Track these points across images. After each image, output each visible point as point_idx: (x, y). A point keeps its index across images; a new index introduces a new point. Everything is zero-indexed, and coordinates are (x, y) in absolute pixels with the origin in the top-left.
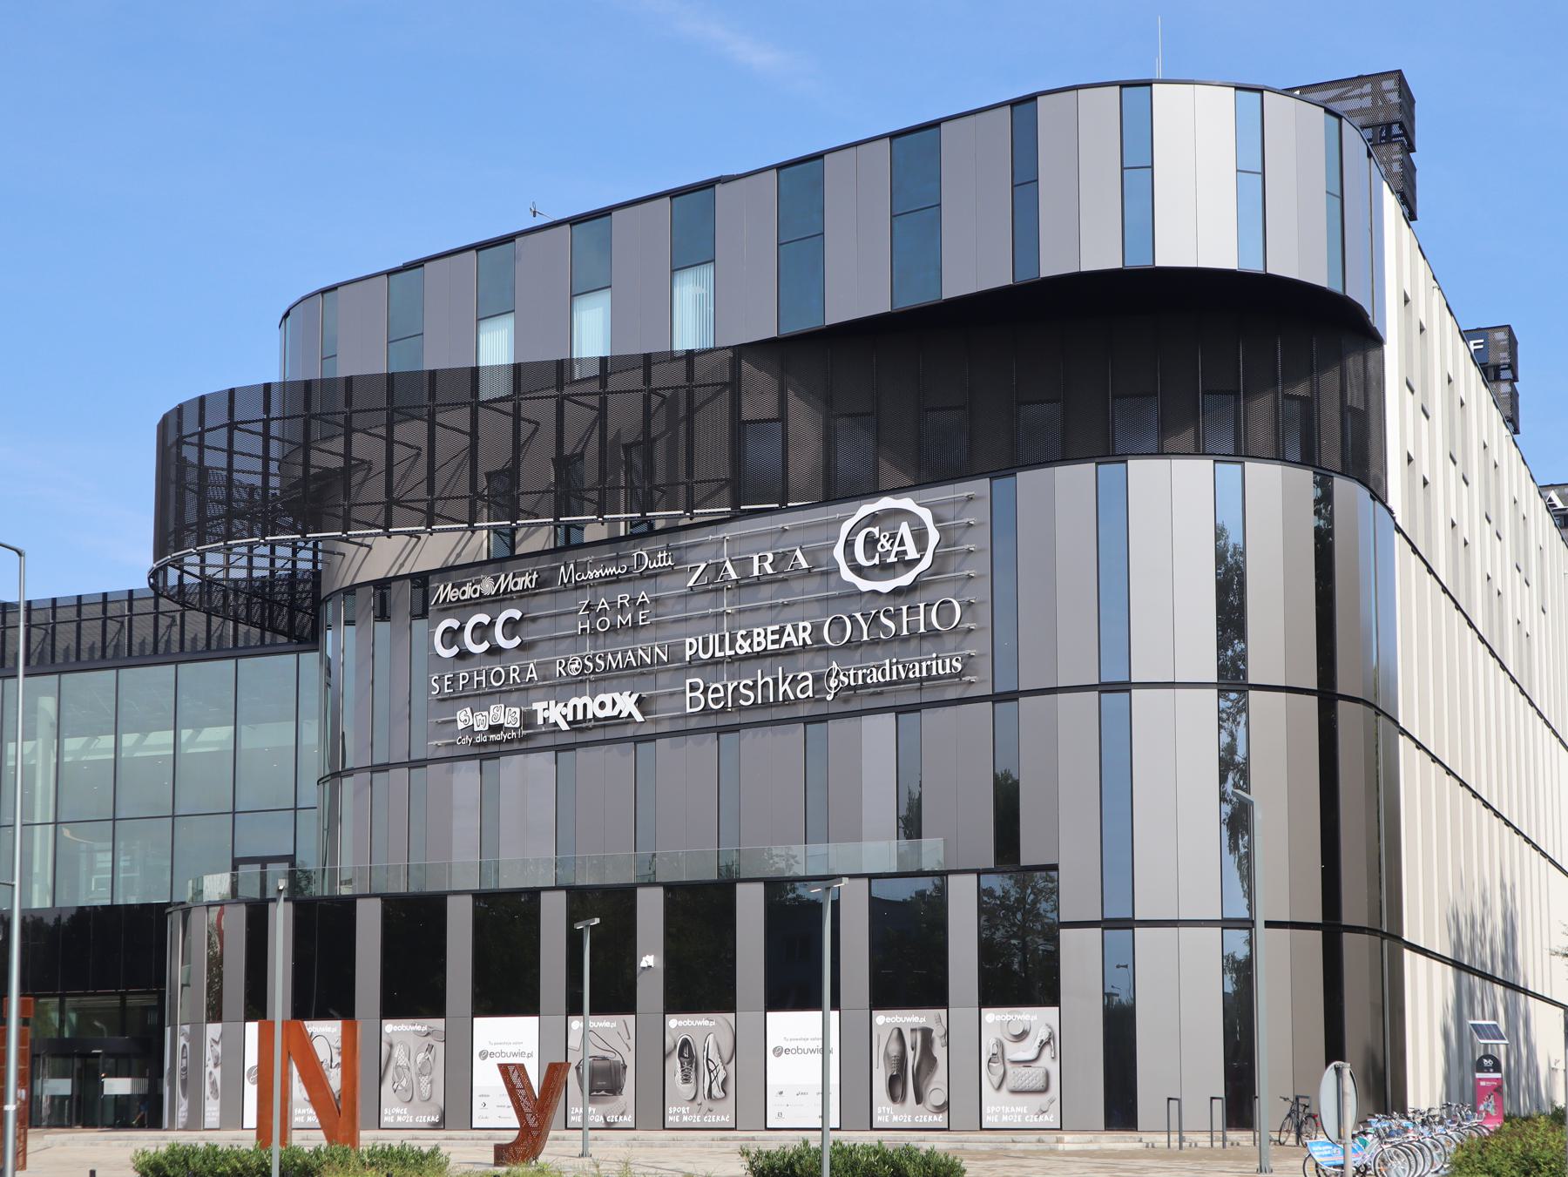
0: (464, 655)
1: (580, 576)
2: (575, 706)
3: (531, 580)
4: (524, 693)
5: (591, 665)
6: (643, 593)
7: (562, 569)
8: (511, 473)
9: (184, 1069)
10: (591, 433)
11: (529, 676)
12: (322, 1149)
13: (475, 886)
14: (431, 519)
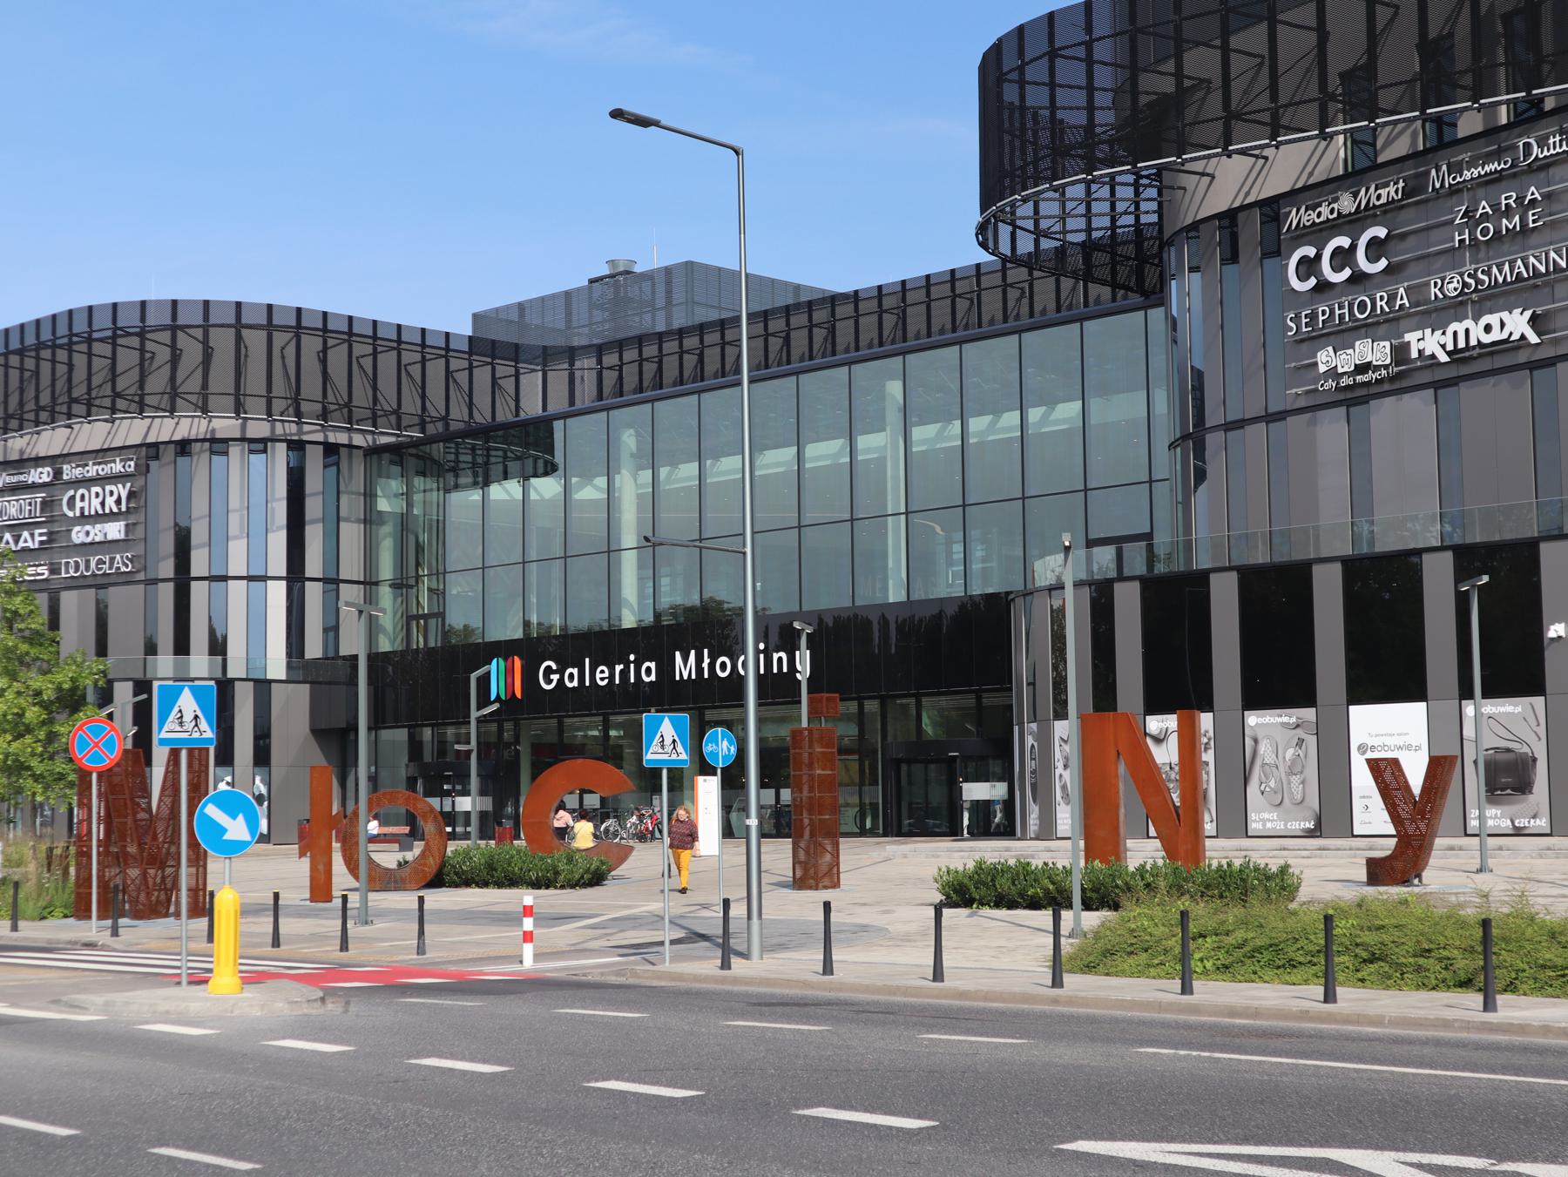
0: (1323, 287)
1: (1454, 179)
2: (1455, 333)
3: (1397, 189)
4: (1394, 324)
5: (1472, 282)
6: (1533, 189)
7: (1433, 172)
8: (1369, 68)
9: (1034, 772)
10: (1458, 15)
11: (1399, 302)
12: (1148, 867)
13: (1347, 551)
14: (1275, 130)
